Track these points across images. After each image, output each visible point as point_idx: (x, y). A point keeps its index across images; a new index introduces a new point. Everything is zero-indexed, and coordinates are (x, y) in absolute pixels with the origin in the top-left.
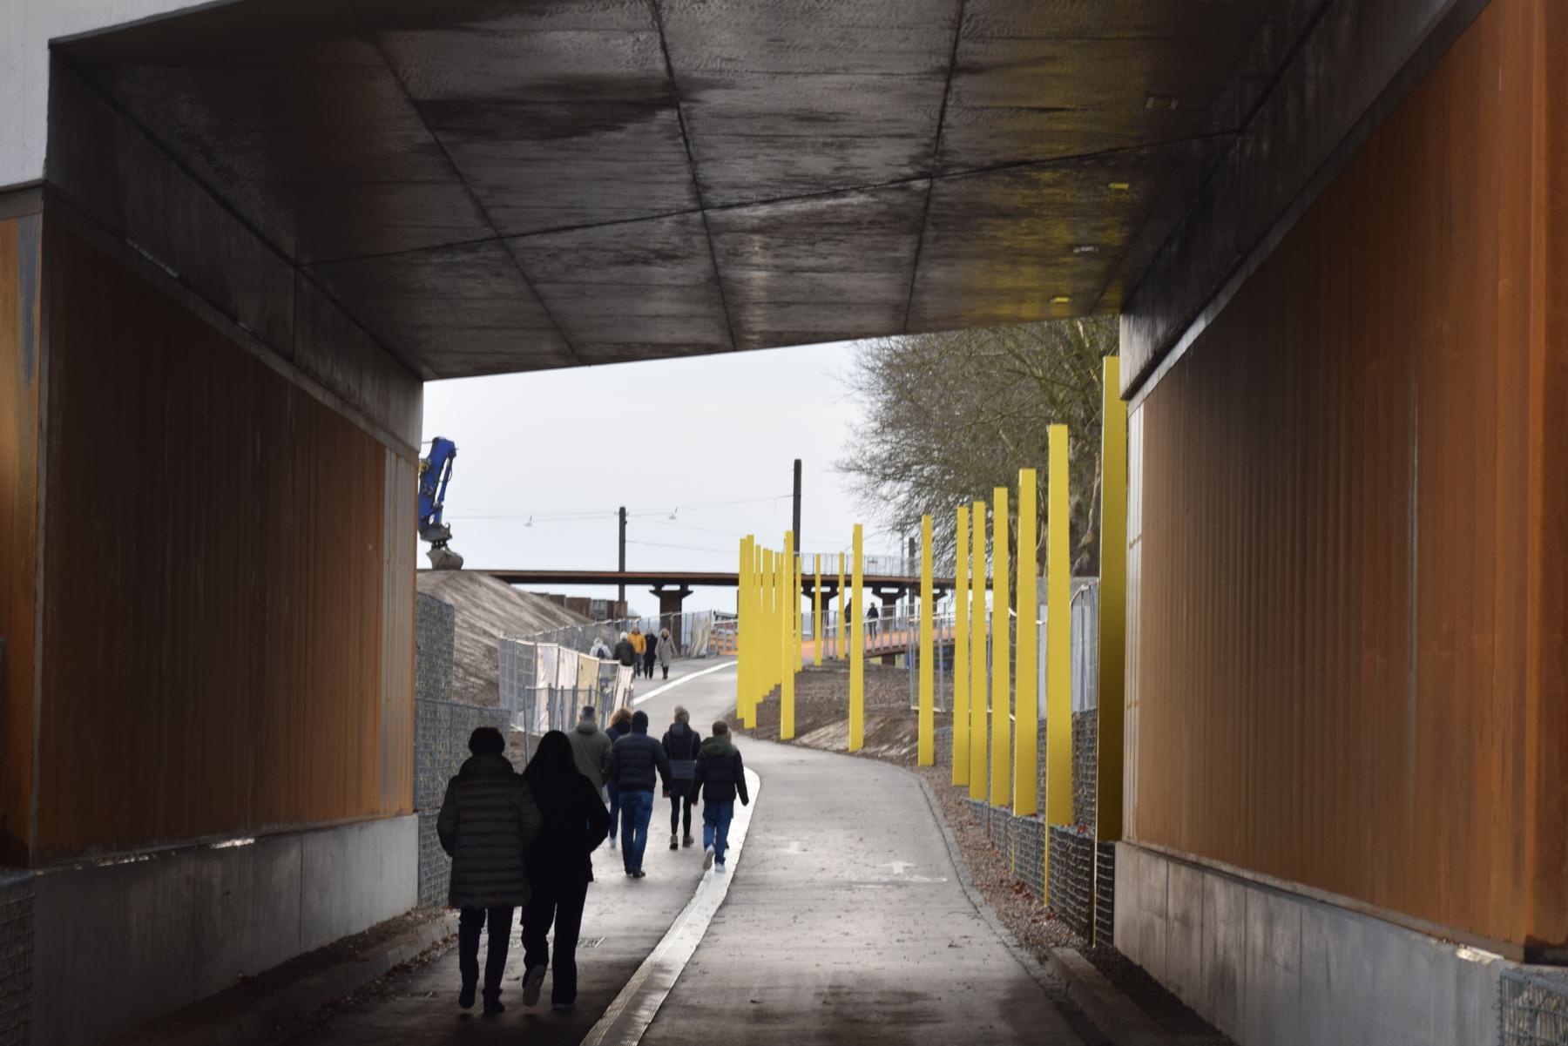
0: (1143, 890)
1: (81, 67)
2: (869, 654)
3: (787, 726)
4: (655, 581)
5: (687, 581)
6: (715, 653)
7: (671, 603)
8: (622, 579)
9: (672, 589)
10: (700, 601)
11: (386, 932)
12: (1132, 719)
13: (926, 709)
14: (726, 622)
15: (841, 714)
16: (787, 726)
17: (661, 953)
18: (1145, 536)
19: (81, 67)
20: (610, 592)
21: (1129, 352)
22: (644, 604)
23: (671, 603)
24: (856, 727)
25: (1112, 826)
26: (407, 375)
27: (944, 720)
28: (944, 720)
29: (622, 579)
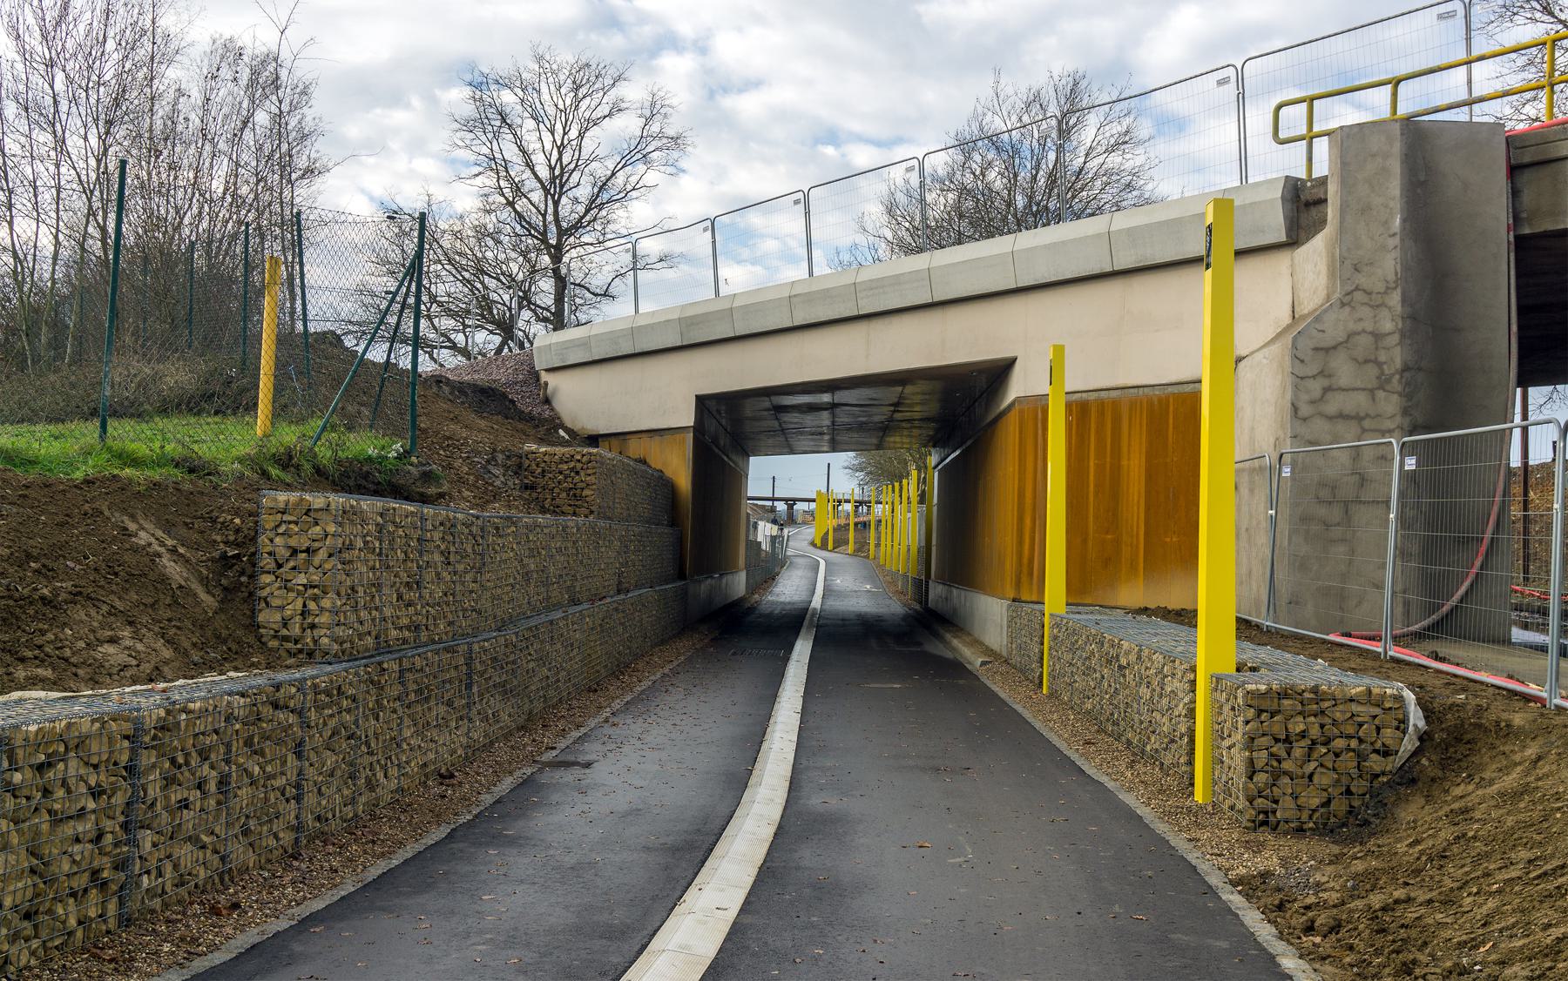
0: (936, 591)
1: (701, 401)
2: (856, 524)
3: (830, 546)
4: (786, 500)
5: (795, 500)
6: (804, 523)
7: (791, 507)
8: (773, 499)
9: (791, 502)
10: (800, 506)
11: (742, 600)
12: (934, 542)
13: (872, 542)
14: (811, 513)
15: (847, 543)
16: (830, 546)
17: (813, 605)
18: (939, 504)
19: (701, 401)
20: (769, 503)
21: (933, 460)
22: (781, 507)
23: (791, 507)
24: (851, 548)
25: (928, 576)
26: (746, 454)
27: (878, 545)
28: (878, 545)
29: (773, 499)
